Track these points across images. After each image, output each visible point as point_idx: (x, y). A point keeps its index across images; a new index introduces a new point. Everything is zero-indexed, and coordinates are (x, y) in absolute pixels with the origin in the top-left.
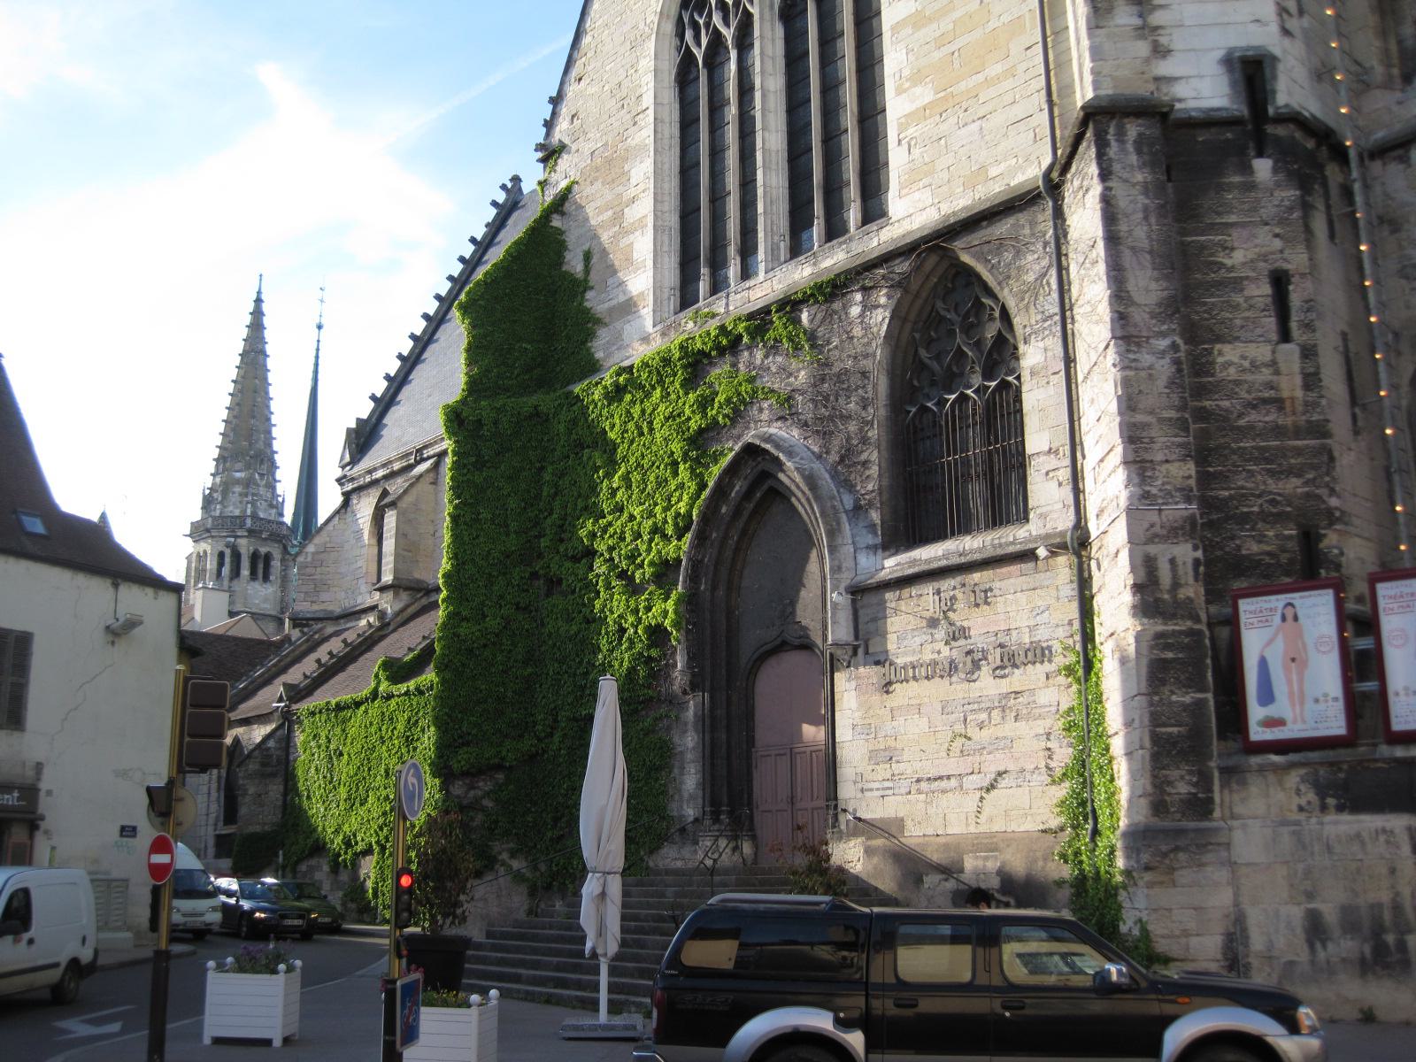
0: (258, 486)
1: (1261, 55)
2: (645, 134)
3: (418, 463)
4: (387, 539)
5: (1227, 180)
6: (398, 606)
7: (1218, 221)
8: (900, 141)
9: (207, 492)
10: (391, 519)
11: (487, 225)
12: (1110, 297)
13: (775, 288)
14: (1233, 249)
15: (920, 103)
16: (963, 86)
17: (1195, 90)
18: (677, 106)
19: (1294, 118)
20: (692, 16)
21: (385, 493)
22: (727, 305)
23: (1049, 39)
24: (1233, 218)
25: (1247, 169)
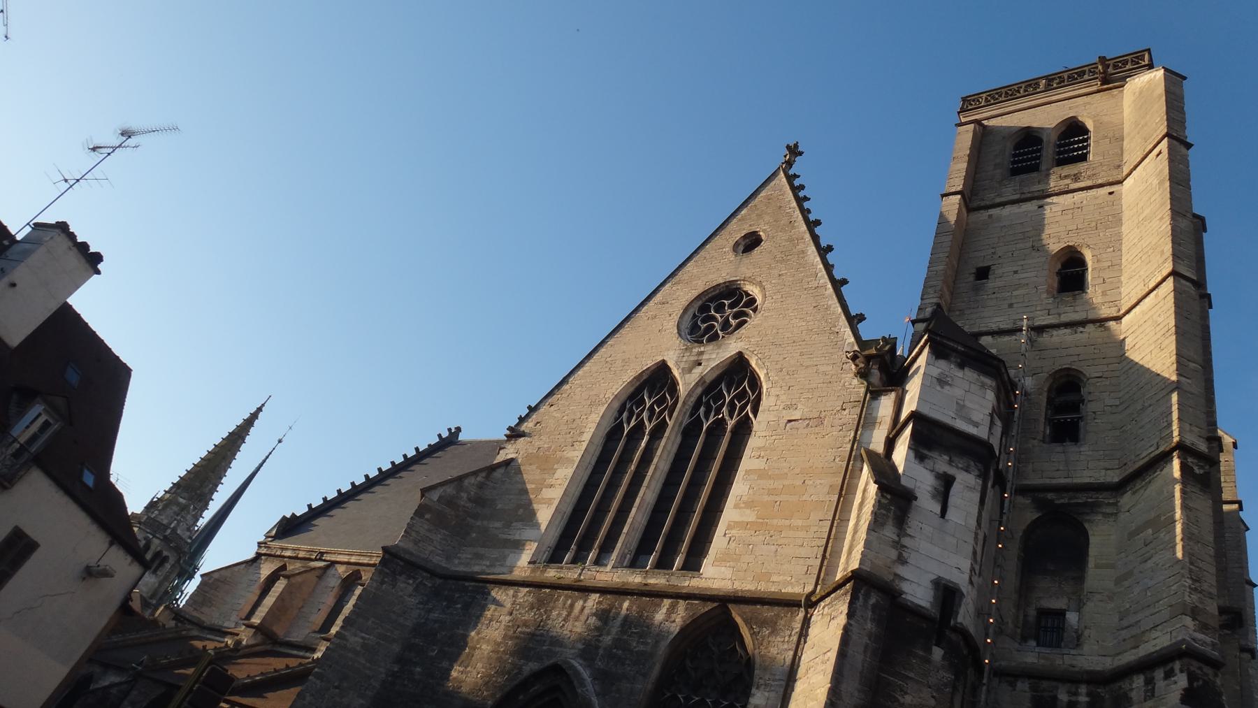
0: (189, 513)
1: (956, 589)
2: (576, 454)
3: (316, 560)
4: (270, 596)
5: (914, 650)
6: (252, 642)
7: (903, 672)
8: (725, 534)
9: (155, 500)
10: (280, 585)
11: (429, 445)
12: (830, 689)
13: (614, 579)
14: (906, 693)
15: (746, 519)
16: (775, 522)
17: (913, 590)
18: (601, 449)
19: (963, 632)
20: (632, 406)
21: (284, 567)
22: (580, 574)
23: (835, 521)
24: (911, 675)
25: (928, 650)
